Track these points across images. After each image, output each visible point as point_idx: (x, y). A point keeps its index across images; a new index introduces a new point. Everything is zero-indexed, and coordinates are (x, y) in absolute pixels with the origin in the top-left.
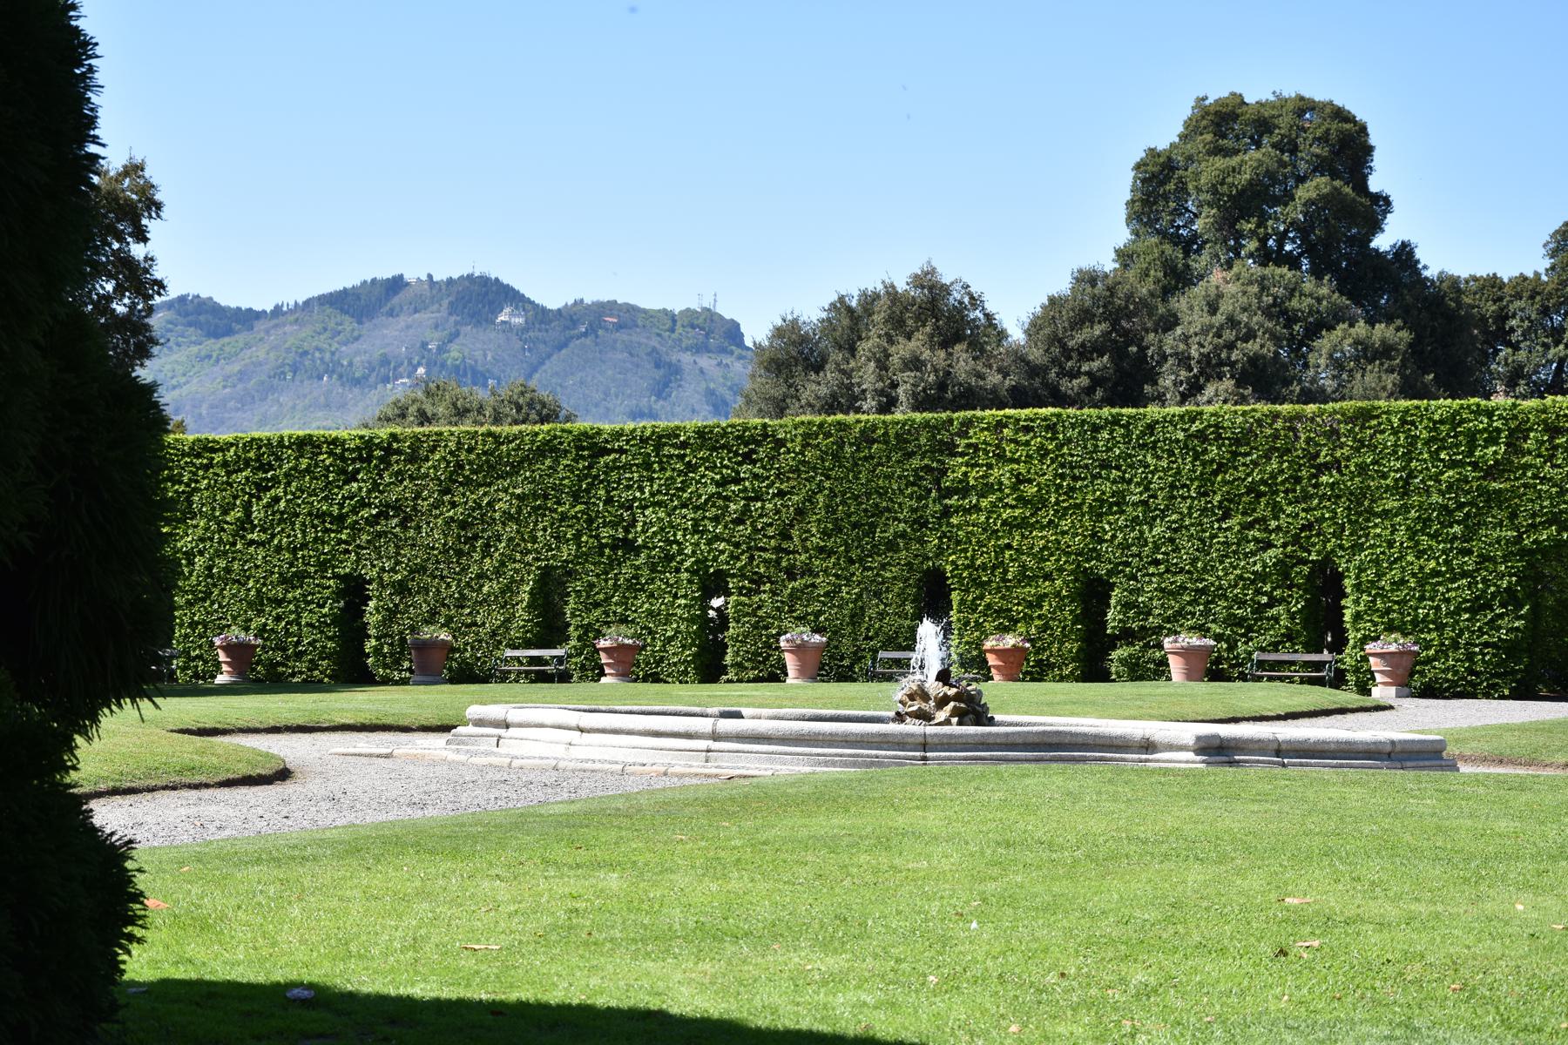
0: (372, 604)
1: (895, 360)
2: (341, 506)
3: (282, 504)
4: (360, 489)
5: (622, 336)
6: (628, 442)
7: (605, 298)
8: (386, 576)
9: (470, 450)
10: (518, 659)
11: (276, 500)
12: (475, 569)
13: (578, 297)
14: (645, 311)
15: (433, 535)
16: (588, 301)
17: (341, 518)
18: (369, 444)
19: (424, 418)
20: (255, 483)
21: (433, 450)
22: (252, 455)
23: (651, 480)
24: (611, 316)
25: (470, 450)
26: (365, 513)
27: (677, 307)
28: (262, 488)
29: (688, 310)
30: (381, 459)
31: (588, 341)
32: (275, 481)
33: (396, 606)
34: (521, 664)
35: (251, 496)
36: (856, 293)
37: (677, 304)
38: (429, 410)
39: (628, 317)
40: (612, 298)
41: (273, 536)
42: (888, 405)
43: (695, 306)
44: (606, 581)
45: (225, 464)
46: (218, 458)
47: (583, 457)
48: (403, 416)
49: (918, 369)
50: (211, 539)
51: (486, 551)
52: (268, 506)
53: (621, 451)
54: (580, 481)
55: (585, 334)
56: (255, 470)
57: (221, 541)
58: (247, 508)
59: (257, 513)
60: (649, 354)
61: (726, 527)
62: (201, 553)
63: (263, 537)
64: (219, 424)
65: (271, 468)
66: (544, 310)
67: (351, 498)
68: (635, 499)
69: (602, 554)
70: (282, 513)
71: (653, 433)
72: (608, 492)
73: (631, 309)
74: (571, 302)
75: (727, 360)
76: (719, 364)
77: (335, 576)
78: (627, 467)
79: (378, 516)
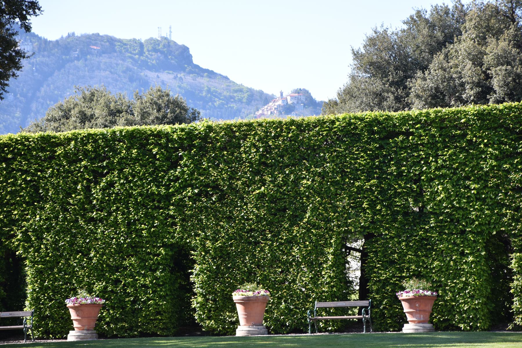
0: (197, 267)
1: (488, 59)
2: (168, 187)
3: (117, 186)
4: (183, 172)
5: (104, 59)
6: (413, 126)
7: (90, 31)
8: (208, 244)
9: (276, 137)
10: (325, 309)
11: (111, 184)
12: (284, 235)
13: (71, 32)
14: (120, 41)
15: (250, 210)
16: (78, 34)
17: (168, 197)
18: (48, 143)
19: (85, 118)
20: (94, 171)
21: (245, 137)
22: (89, 147)
23: (437, 156)
24: (95, 45)
25: (276, 137)
26: (189, 192)
27: (143, 37)
28: (98, 175)
29: (151, 39)
30: (201, 148)
31: (80, 63)
32: (110, 169)
33: (218, 267)
34: (329, 313)
35: (88, 181)
36: (429, 9)
37: (143, 35)
38: (89, 112)
39: (110, 45)
40: (95, 32)
41: (110, 214)
42: (482, 97)
43: (156, 36)
44: (399, 243)
45: (66, 155)
46: (59, 151)
47: (374, 140)
48: (67, 116)
49: (508, 64)
50: (56, 218)
51: (295, 220)
52: (103, 189)
53: (407, 134)
54: (373, 160)
55: (78, 59)
56: (92, 160)
57: (65, 218)
58: (87, 189)
59: (96, 192)
60: (124, 72)
61: (506, 194)
62: (48, 230)
63: (104, 214)
64: (236, 113)
65: (107, 158)
66: (45, 41)
67: (175, 181)
68: (422, 173)
69: (395, 220)
70: (117, 194)
71: (436, 116)
72: (398, 168)
73: (111, 41)
74: (65, 35)
75: (181, 75)
76: (175, 78)
77: (164, 245)
78: (415, 147)
79: (199, 195)
